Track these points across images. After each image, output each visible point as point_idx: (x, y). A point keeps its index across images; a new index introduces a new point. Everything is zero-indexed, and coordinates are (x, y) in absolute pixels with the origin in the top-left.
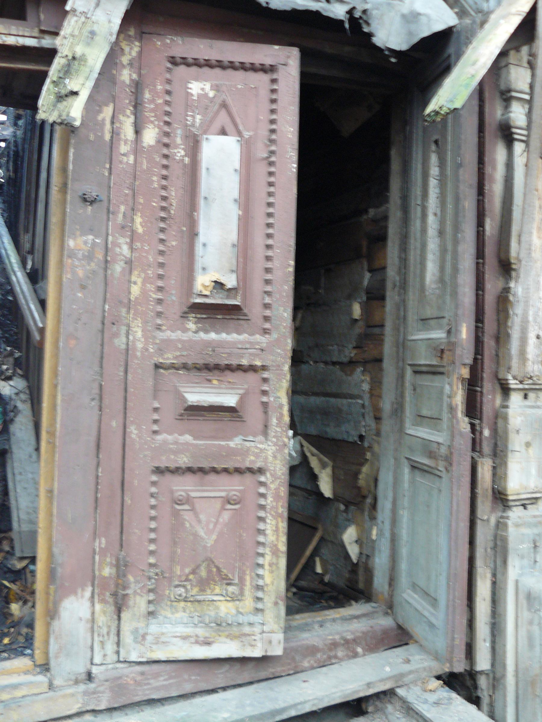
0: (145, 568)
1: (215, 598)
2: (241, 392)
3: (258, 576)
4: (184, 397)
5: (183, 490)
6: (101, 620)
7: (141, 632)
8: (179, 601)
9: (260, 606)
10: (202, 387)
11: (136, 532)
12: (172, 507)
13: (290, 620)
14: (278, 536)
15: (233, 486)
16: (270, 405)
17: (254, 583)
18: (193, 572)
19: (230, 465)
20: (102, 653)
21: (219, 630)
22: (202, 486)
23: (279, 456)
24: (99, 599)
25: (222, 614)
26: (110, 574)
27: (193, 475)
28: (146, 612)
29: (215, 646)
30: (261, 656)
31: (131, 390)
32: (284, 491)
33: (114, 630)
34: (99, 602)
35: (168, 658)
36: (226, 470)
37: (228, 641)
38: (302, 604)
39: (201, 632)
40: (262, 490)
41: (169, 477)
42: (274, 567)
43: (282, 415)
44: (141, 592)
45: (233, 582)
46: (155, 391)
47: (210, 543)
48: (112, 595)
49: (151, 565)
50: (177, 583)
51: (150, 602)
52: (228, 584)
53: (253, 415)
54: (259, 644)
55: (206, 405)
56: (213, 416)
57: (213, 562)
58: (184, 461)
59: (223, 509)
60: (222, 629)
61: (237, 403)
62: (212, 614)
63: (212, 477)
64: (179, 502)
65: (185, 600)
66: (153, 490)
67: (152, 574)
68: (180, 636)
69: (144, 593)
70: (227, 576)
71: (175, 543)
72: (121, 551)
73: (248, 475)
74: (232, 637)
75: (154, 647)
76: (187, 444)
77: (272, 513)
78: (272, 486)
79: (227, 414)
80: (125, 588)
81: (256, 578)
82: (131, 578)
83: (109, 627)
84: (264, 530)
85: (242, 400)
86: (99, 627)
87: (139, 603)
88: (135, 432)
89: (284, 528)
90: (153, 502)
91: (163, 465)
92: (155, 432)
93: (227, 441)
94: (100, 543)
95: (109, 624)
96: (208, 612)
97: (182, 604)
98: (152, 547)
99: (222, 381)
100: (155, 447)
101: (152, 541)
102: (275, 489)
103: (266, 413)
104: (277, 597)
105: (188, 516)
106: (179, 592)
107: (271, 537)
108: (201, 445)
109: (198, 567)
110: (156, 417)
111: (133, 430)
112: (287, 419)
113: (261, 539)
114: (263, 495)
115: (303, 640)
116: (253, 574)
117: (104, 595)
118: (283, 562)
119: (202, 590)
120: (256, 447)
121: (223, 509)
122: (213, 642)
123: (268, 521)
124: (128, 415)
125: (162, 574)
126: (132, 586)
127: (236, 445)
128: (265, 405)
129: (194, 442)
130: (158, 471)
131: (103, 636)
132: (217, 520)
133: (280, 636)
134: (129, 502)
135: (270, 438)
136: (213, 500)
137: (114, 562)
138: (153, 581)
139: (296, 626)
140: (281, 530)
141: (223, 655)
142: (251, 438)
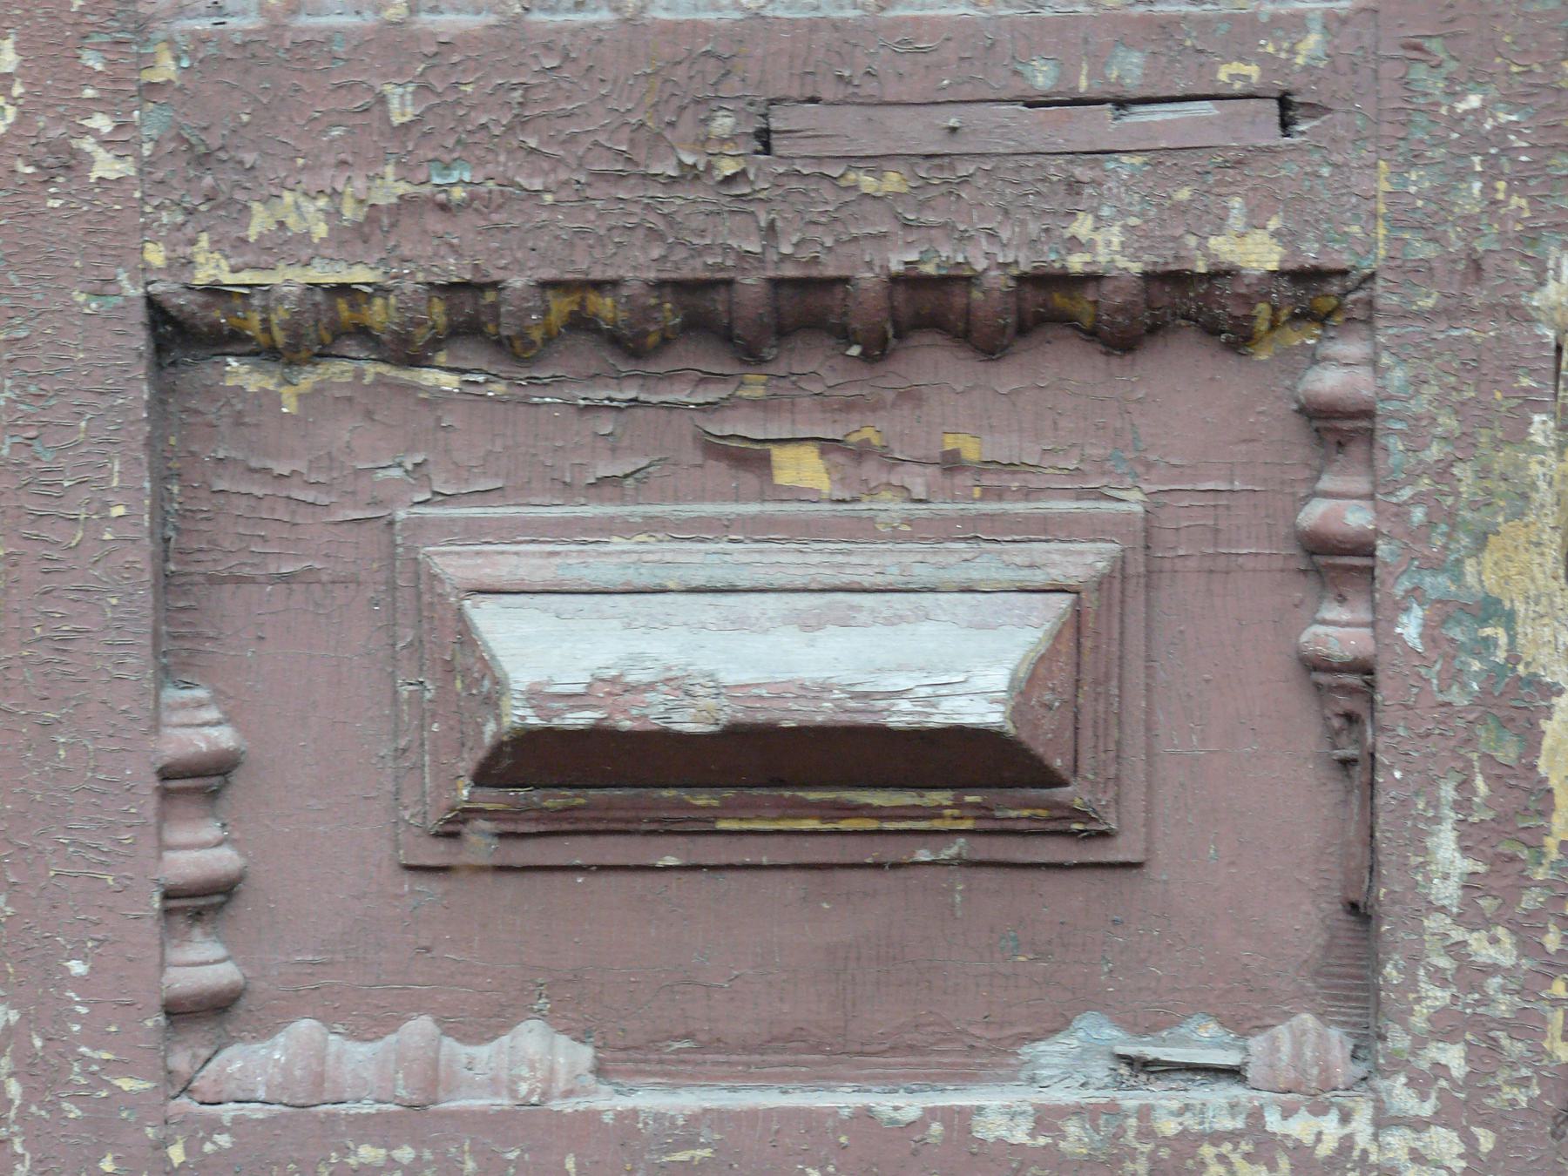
2: (1082, 561)
4: (466, 636)
10: (652, 526)
46: (166, 583)
55: (687, 722)
61: (1025, 690)
76: (529, 1124)
85: (1090, 641)
92: (205, 1013)
93: (965, 1077)
99: (861, 453)
103: (1356, 771)
108: (689, 1130)
110: (200, 850)
127: (1046, 1119)
129: (608, 1101)
135: (1398, 1040)
142: (1204, 1042)
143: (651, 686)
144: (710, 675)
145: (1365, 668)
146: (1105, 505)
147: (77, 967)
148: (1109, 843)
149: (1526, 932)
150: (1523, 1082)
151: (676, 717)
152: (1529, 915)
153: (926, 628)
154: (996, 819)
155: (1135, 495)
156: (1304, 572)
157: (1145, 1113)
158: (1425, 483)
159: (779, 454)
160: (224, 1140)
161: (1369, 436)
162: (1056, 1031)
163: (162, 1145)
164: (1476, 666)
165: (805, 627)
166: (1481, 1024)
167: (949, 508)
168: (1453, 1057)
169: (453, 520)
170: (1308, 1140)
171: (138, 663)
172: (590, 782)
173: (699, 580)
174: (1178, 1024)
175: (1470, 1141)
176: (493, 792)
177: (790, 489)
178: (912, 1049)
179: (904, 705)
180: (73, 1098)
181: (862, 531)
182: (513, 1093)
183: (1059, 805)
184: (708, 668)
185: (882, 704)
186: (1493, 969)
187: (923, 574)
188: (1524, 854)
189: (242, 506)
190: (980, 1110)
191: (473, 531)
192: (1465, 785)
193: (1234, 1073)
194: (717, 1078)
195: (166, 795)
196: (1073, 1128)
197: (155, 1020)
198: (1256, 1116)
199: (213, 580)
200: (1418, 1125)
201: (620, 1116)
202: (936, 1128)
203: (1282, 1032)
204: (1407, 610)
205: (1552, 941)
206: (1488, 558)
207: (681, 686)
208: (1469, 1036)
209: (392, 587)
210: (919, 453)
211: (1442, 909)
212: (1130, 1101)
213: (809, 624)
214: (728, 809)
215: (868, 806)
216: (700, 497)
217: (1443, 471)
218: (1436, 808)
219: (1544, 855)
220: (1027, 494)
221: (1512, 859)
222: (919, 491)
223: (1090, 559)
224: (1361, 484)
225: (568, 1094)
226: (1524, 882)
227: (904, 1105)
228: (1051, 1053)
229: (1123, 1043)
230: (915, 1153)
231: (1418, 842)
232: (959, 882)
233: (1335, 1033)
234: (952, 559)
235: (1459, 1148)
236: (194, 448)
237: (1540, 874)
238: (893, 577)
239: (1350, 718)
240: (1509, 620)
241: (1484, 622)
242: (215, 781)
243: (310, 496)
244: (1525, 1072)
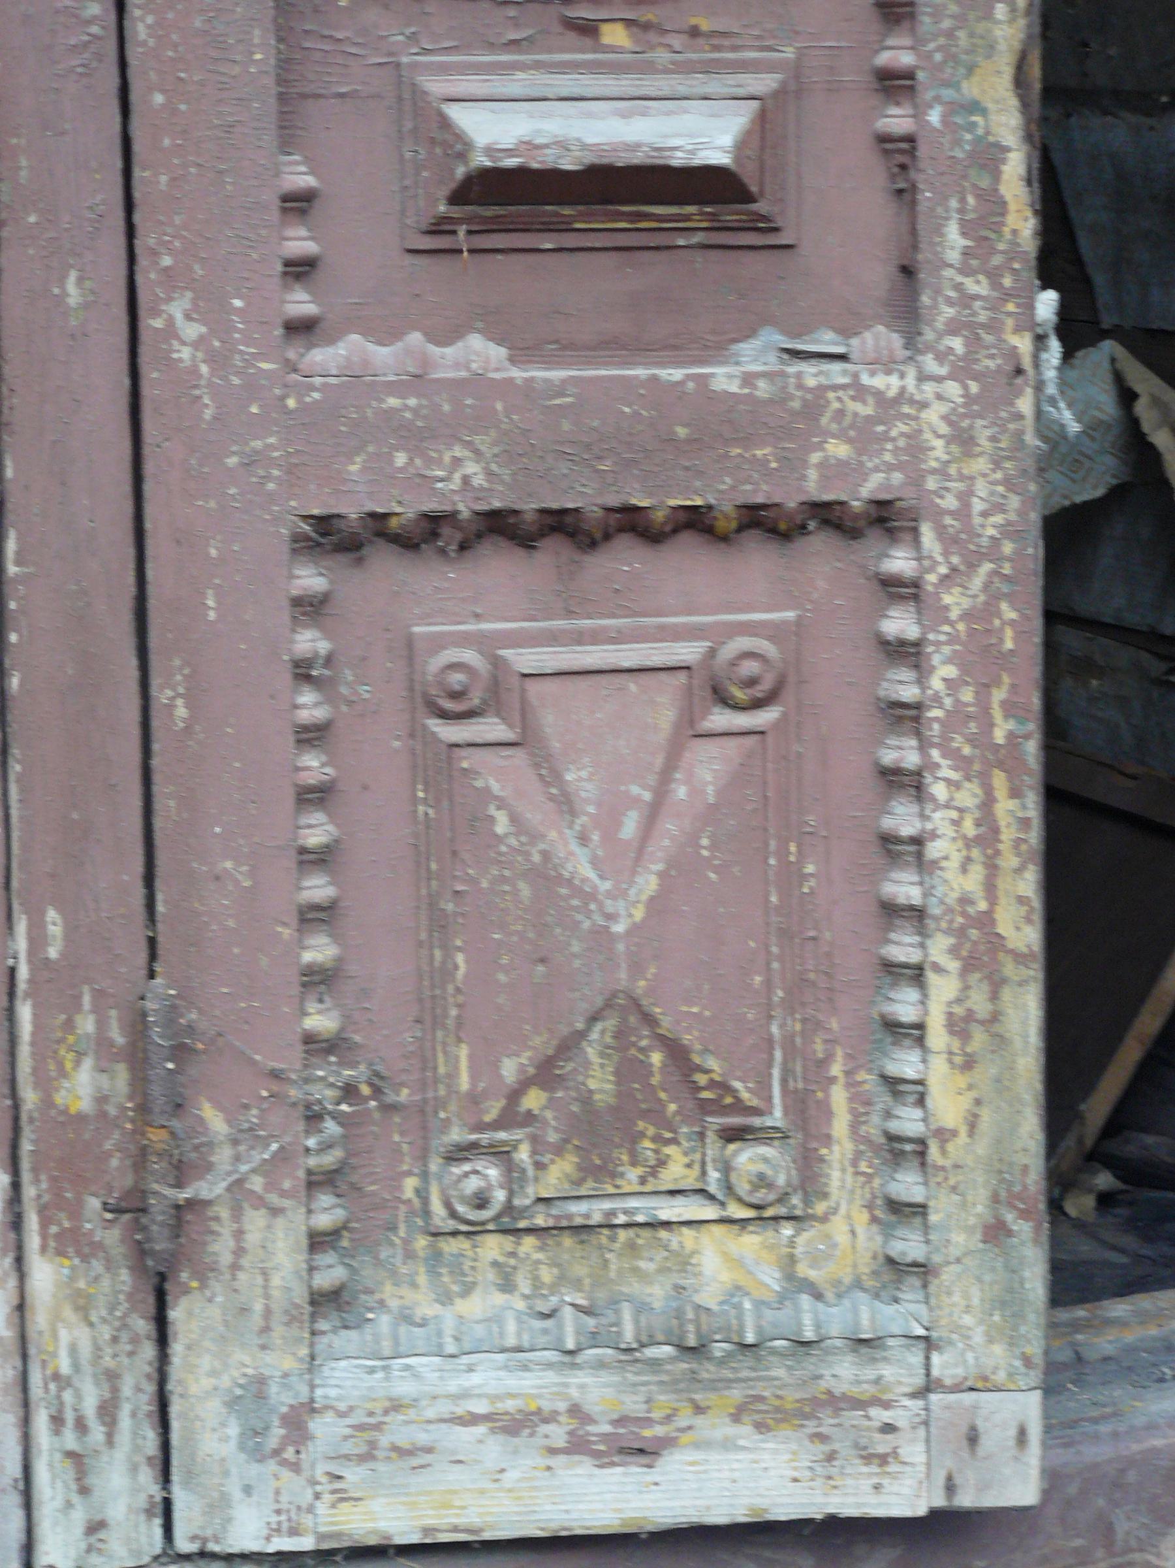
0: (291, 1060)
1: (670, 1210)
2: (765, 83)
3: (893, 1084)
4: (445, 123)
5: (465, 640)
6: (66, 1340)
7: (282, 1398)
8: (475, 1231)
9: (909, 1245)
10: (538, 66)
11: (231, 872)
12: (415, 732)
13: (1076, 1326)
14: (992, 868)
15: (736, 606)
16: (923, 151)
17: (873, 1128)
18: (545, 1074)
19: (720, 492)
20: (79, 1516)
21: (693, 1378)
22: (570, 613)
23: (983, 433)
24: (44, 1236)
25: (709, 1297)
26: (101, 1099)
27: (520, 552)
28: (300, 1296)
29: (673, 1463)
30: (921, 1511)
31: (151, 99)
32: (1018, 626)
33: (136, 1396)
34: (44, 1249)
35: (427, 1531)
36: (695, 522)
37: (744, 1432)
38: (1146, 1251)
39: (599, 1391)
40: (899, 623)
41: (387, 569)
42: (979, 1039)
43: (995, 205)
44: (270, 1186)
45: (757, 1121)
46: (282, 98)
47: (627, 916)
48: (118, 1211)
49: (316, 1046)
50: (457, 1135)
51: (318, 1241)
52: (733, 1135)
53: (834, 209)
54: (914, 1451)
55: (567, 165)
56: (614, 223)
57: (649, 1020)
58: (465, 477)
59: (689, 731)
60: (708, 1371)
61: (740, 147)
62: (657, 1293)
63: (625, 560)
64: (449, 705)
65: (510, 1226)
66: (309, 641)
67: (326, 1095)
68: (487, 1418)
69: (284, 1194)
70: (724, 1087)
71: (440, 925)
72: (152, 975)
73: (819, 544)
74: (762, 1415)
75: (353, 1475)
76: (476, 383)
77: (958, 741)
78: (954, 600)
79: (691, 209)
80: (181, 1173)
81: (883, 1099)
82: (216, 1122)
83: (112, 1377)
84: (917, 841)
85: (768, 127)
86: (56, 1377)
87: (266, 1250)
88: (192, 331)
89: (1025, 823)
90: (310, 706)
91: (352, 509)
92: (301, 329)
93: (702, 362)
94: (37, 940)
95: (108, 1361)
96: (634, 1287)
97: (493, 1247)
98: (319, 950)
99: (646, 27)
100: (304, 408)
101: (316, 916)
102: (966, 616)
103: (905, 195)
104: (995, 1199)
105: (499, 777)
106: (473, 1184)
107: (956, 879)
108: (560, 389)
109: (570, 1045)
110: (299, 242)
111: (177, 322)
112: (1022, 225)
113: (904, 887)
114: (906, 653)
115: (1151, 1427)
116: (862, 1076)
117: (76, 1212)
118: (1025, 1011)
119: (597, 1170)
120: (860, 392)
121: (689, 731)
122: (667, 1443)
123: (939, 791)
124: (146, 240)
125: (377, 1091)
126: (223, 1156)
127: (748, 379)
128: (900, 152)
129: (517, 374)
130: (328, 537)
131: (81, 1426)
132: (661, 792)
133: (1028, 1406)
134: (181, 711)
135: (929, 335)
136: (632, 685)
137: (118, 1037)
138: (331, 1127)
139: (1106, 1359)
140: (1008, 834)
141: (722, 1510)
142: (827, 341)
143: (546, 146)
144: (578, 140)
145: (910, 139)
146: (776, 54)
147: (238, 303)
148: (780, 234)
149: (994, 276)
150: (992, 357)
151: (560, 161)
152: (997, 268)
153: (686, 116)
154: (719, 221)
155: (791, 49)
156: (877, 90)
157: (799, 375)
158: (942, 41)
159: (605, 28)
160: (316, 395)
161: (912, 16)
162: (748, 337)
163: (283, 398)
164: (968, 137)
165: (624, 117)
166: (971, 326)
167: (694, 56)
168: (957, 344)
169: (432, 63)
170: (882, 387)
171: (269, 139)
172: (514, 200)
173: (565, 93)
174: (811, 332)
175: (966, 387)
176: (456, 208)
177: (607, 46)
178: (675, 347)
179: (679, 154)
180: (237, 374)
181: (648, 68)
182: (468, 369)
183: (756, 213)
184: (576, 135)
185: (668, 153)
186: (976, 297)
187: (682, 90)
188: (993, 236)
189: (318, 56)
190: (712, 375)
191: (444, 69)
192: (963, 200)
193: (842, 357)
194: (571, 364)
195: (284, 210)
196: (761, 383)
197: (279, 332)
198: (856, 376)
199: (304, 96)
200: (939, 379)
201: (526, 380)
202: (691, 385)
203: (868, 335)
204: (931, 107)
205: (1007, 282)
206: (975, 79)
207: (562, 145)
208: (965, 333)
209: (400, 99)
210: (676, 27)
211: (951, 266)
212: (791, 370)
213: (624, 115)
214: (581, 217)
215: (654, 215)
216: (562, 50)
217: (950, 34)
218: (947, 211)
219: (1002, 236)
220: (734, 48)
221: (986, 239)
222: (678, 47)
223: (768, 82)
224: (907, 41)
225: (497, 370)
226: (993, 251)
227: (676, 374)
228: (746, 348)
229: (783, 342)
230: (680, 398)
231: (939, 230)
232: (699, 257)
233: (895, 336)
234: (694, 83)
235: (961, 392)
236: (292, 24)
237: (1001, 246)
238: (666, 92)
239: (903, 167)
240: (984, 112)
241: (971, 113)
242: (305, 204)
243: (353, 50)
244: (994, 351)
